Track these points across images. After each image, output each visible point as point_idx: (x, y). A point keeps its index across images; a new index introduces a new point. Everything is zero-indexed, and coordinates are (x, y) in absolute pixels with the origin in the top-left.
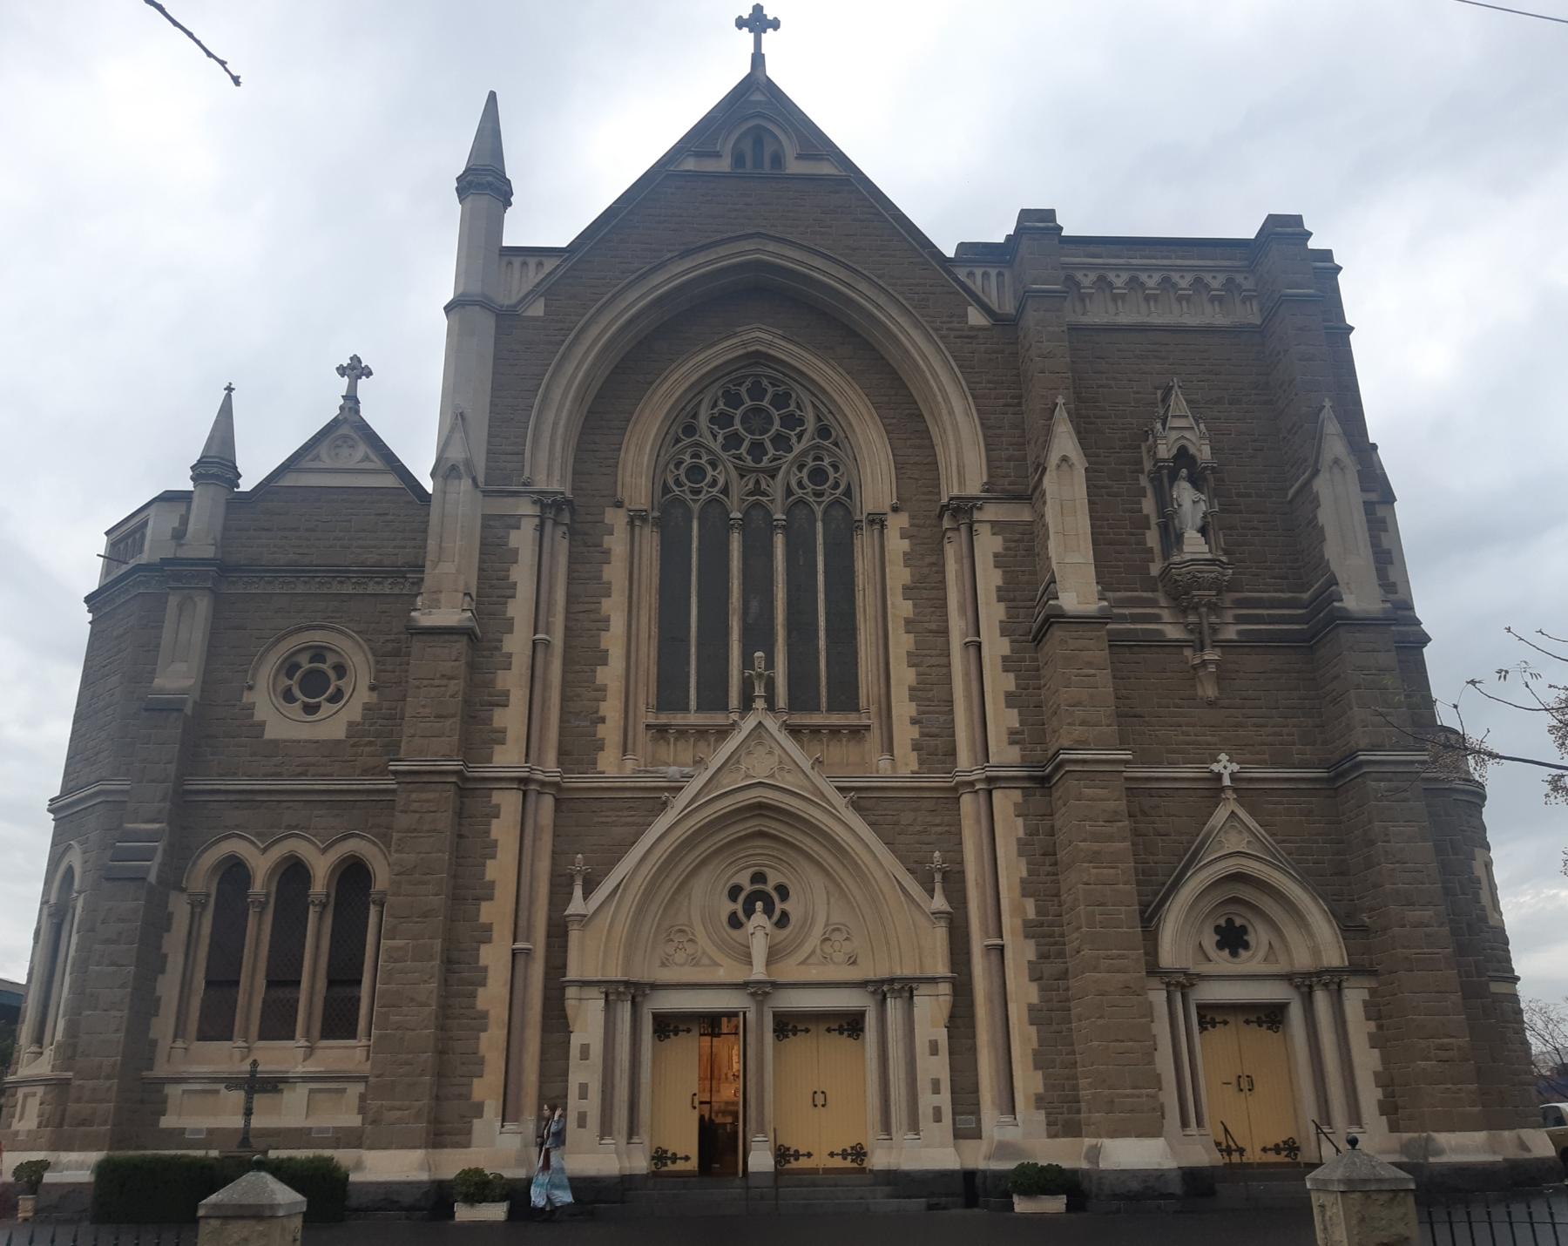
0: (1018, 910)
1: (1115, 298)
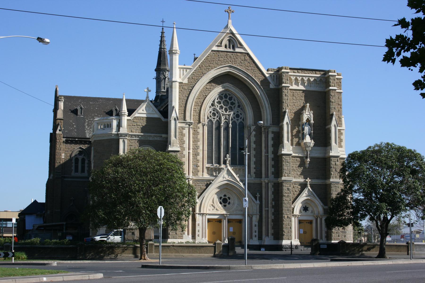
0: (272, 203)
1: (400, 168)
